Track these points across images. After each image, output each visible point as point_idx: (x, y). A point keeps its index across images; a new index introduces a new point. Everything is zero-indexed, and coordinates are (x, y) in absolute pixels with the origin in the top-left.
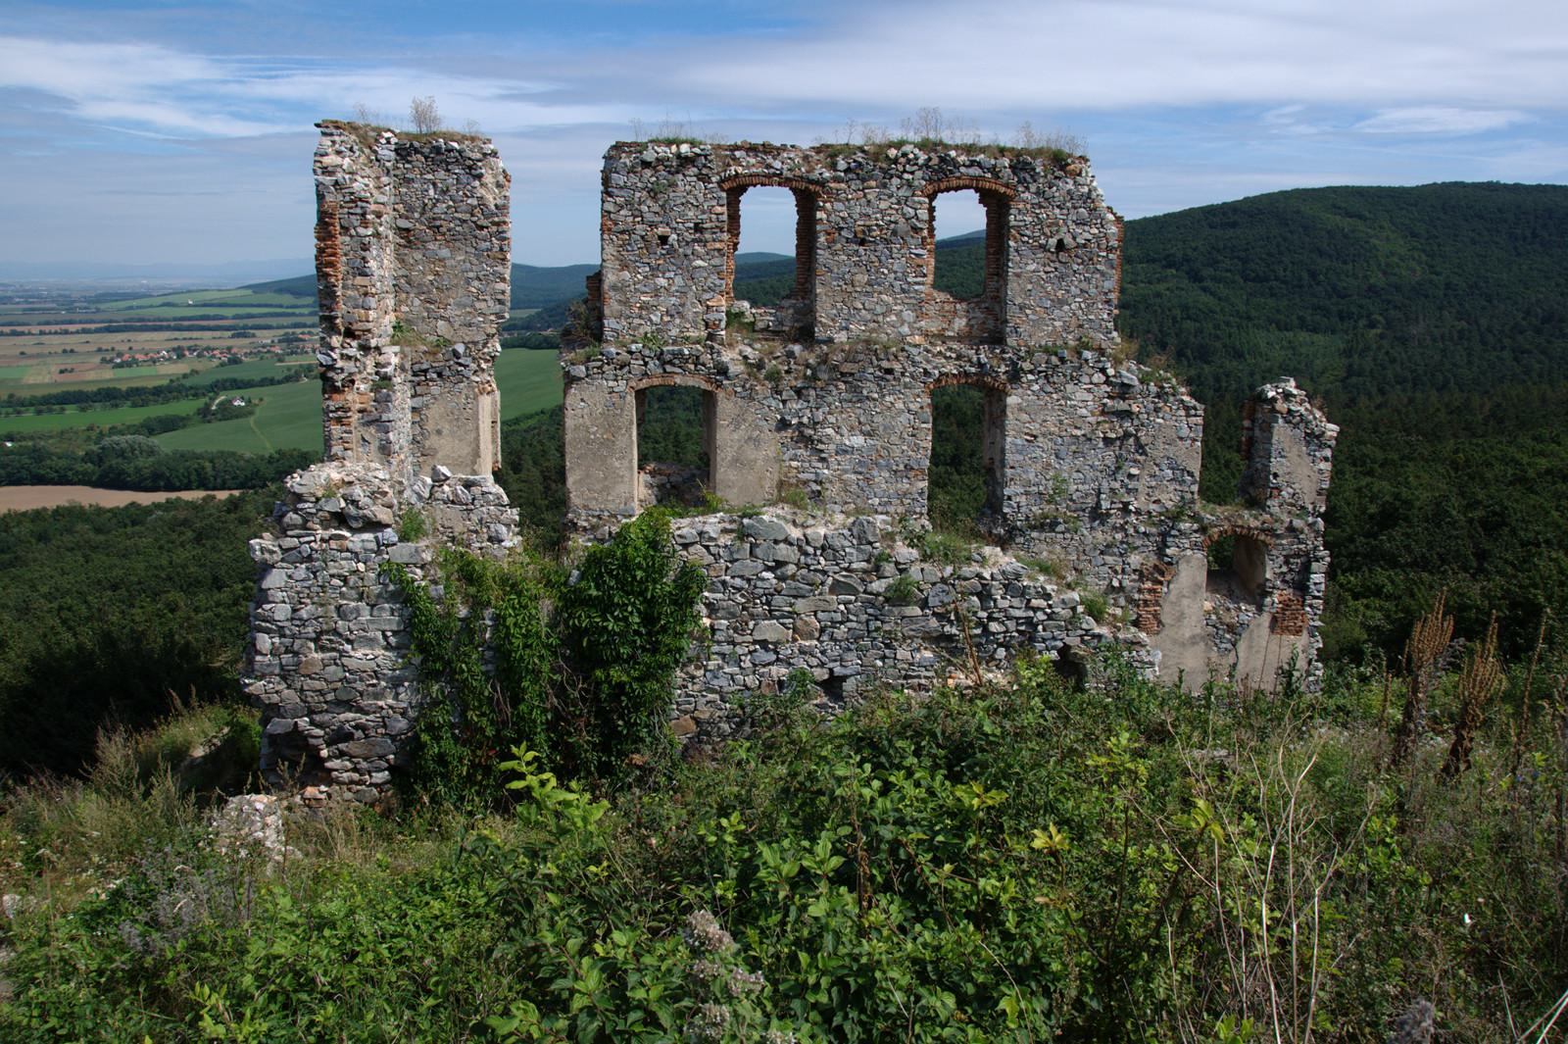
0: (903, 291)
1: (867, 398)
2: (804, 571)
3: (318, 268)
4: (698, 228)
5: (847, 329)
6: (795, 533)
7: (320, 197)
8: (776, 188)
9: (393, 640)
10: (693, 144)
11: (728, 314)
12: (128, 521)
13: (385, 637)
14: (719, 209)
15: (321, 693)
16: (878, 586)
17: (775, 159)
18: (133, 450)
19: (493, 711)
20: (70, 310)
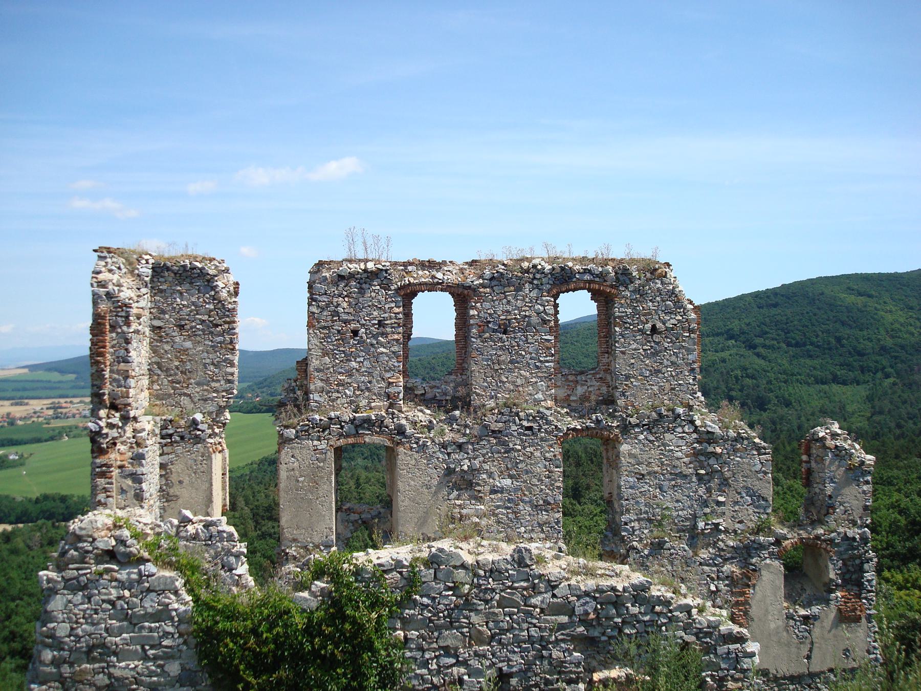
4: (381, 324)
7: (95, 303)
8: (439, 293)
11: (405, 387)
14: (397, 310)
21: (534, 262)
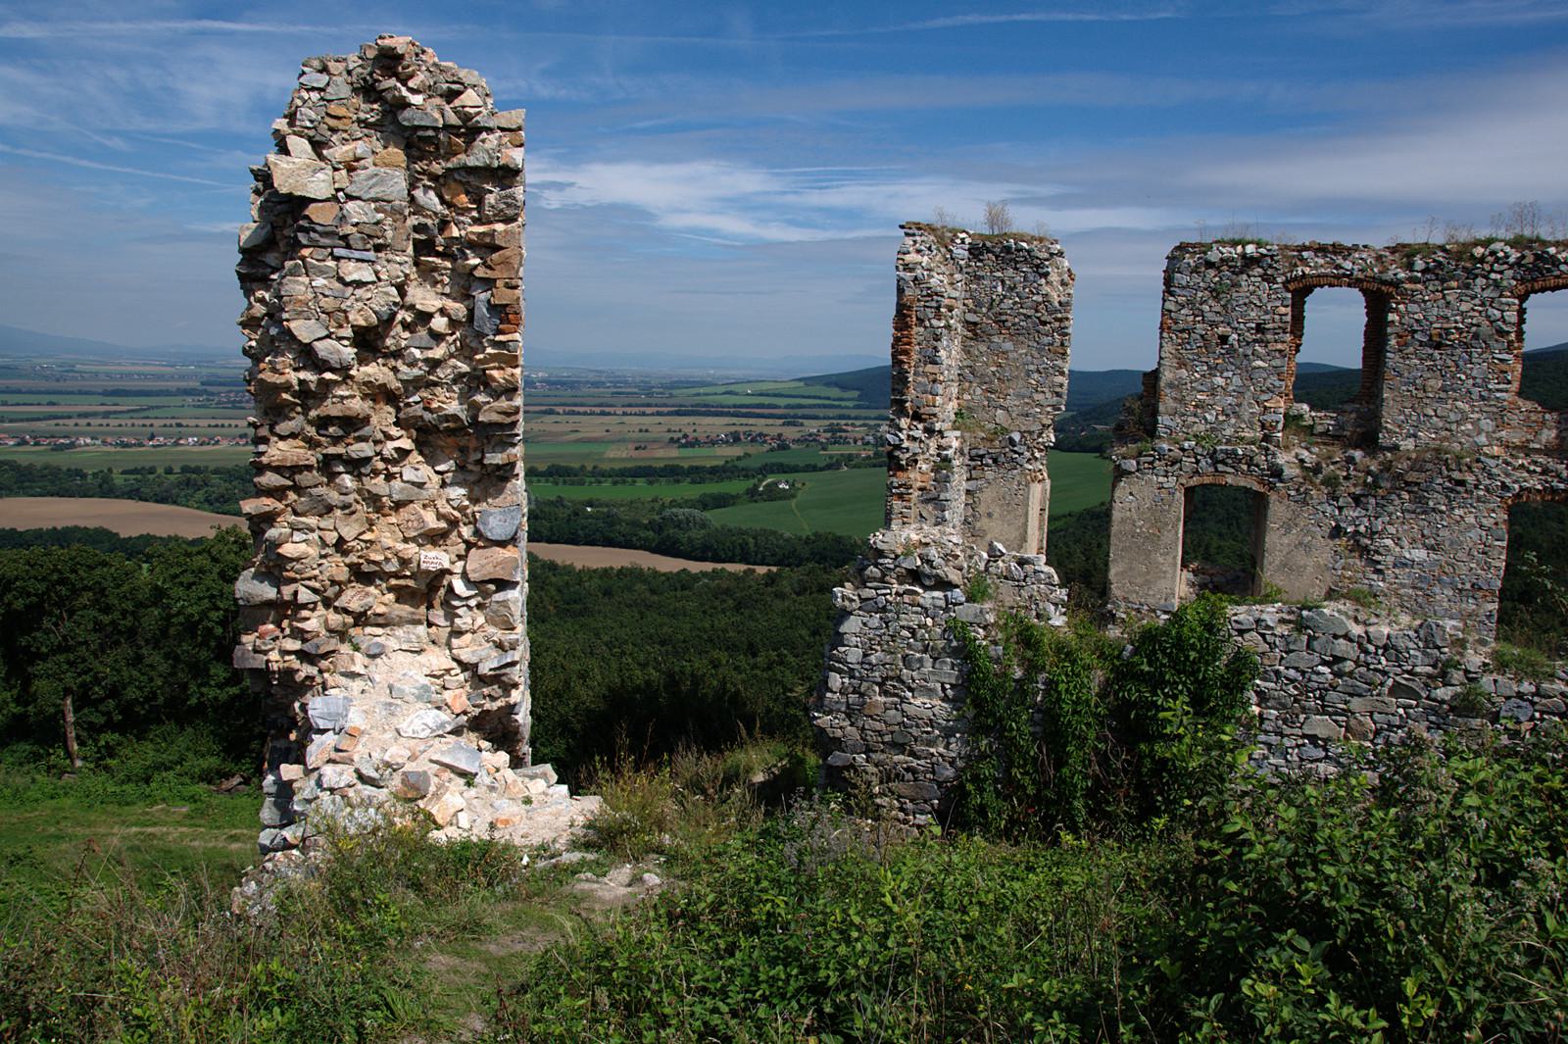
0: (1483, 398)
1: (1434, 510)
2: (1363, 670)
3: (894, 356)
4: (1260, 329)
5: (1415, 436)
6: (1357, 630)
7: (900, 291)
9: (950, 693)
10: (1259, 245)
11: (1286, 416)
12: (678, 585)
13: (944, 690)
14: (1283, 310)
15: (880, 733)
16: (1443, 693)
17: (1345, 259)
18: (688, 522)
19: (1036, 771)
20: (649, 395)
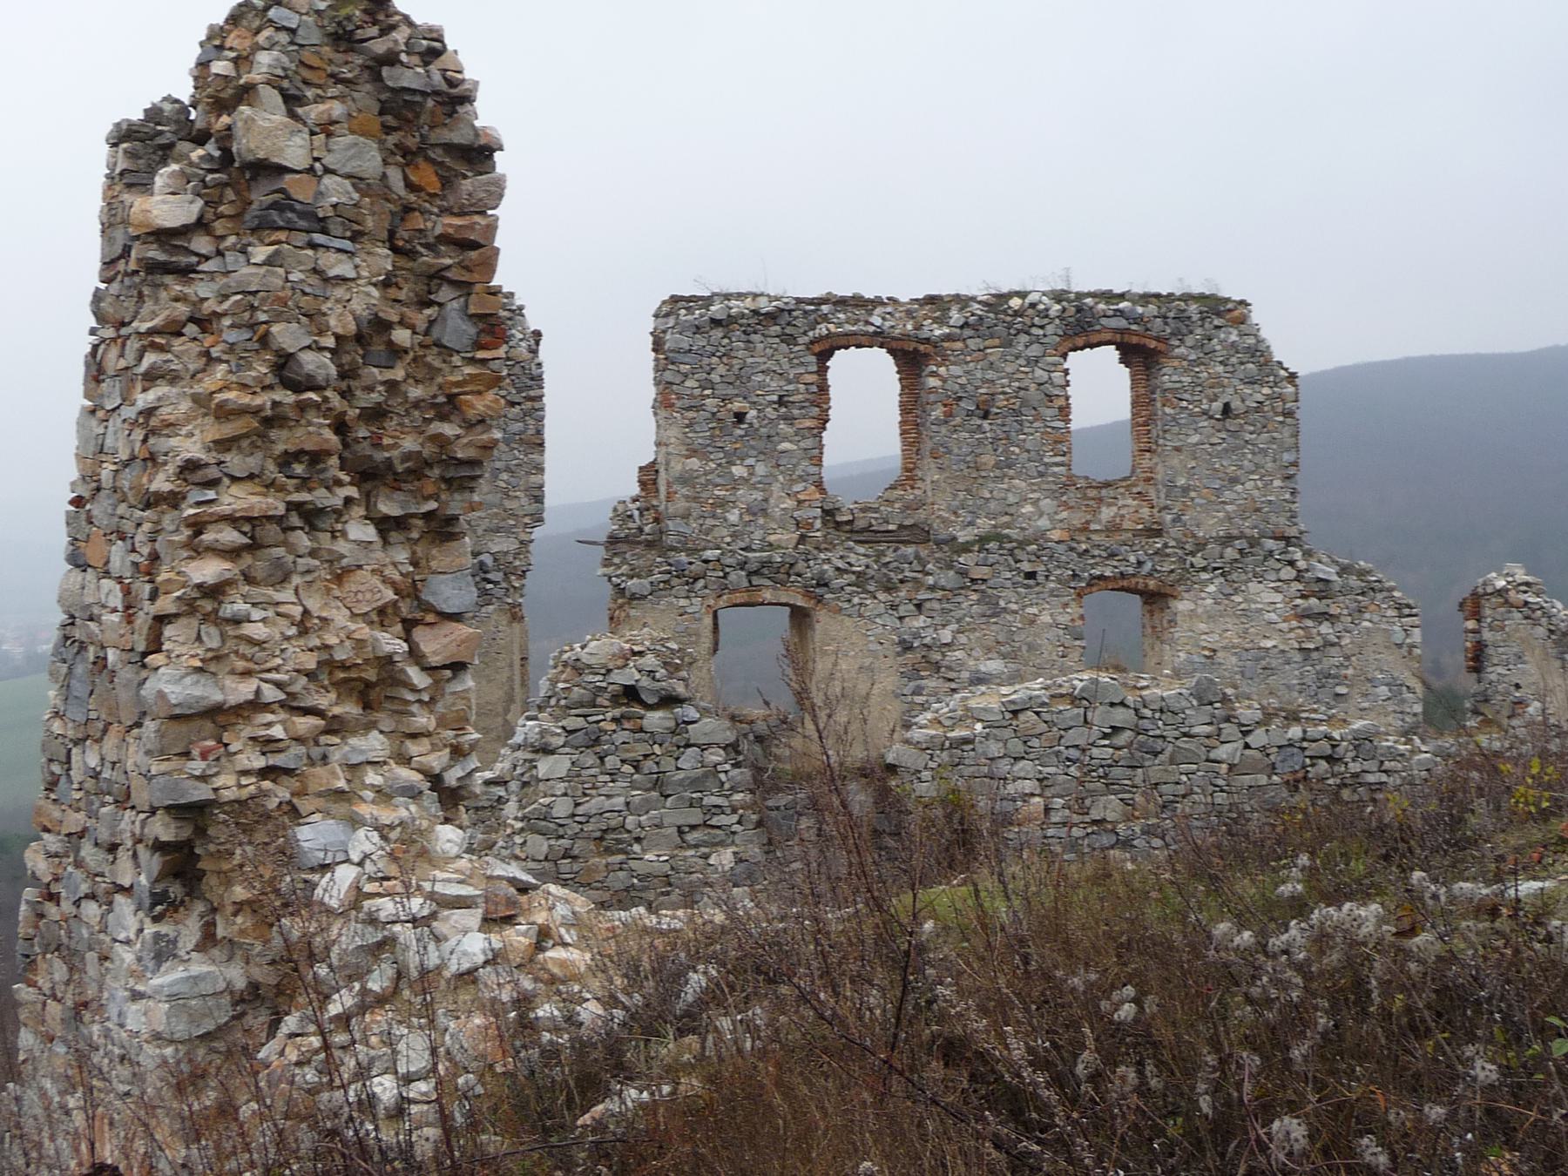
0: (1041, 475)
4: (781, 402)
21: (1032, 298)
